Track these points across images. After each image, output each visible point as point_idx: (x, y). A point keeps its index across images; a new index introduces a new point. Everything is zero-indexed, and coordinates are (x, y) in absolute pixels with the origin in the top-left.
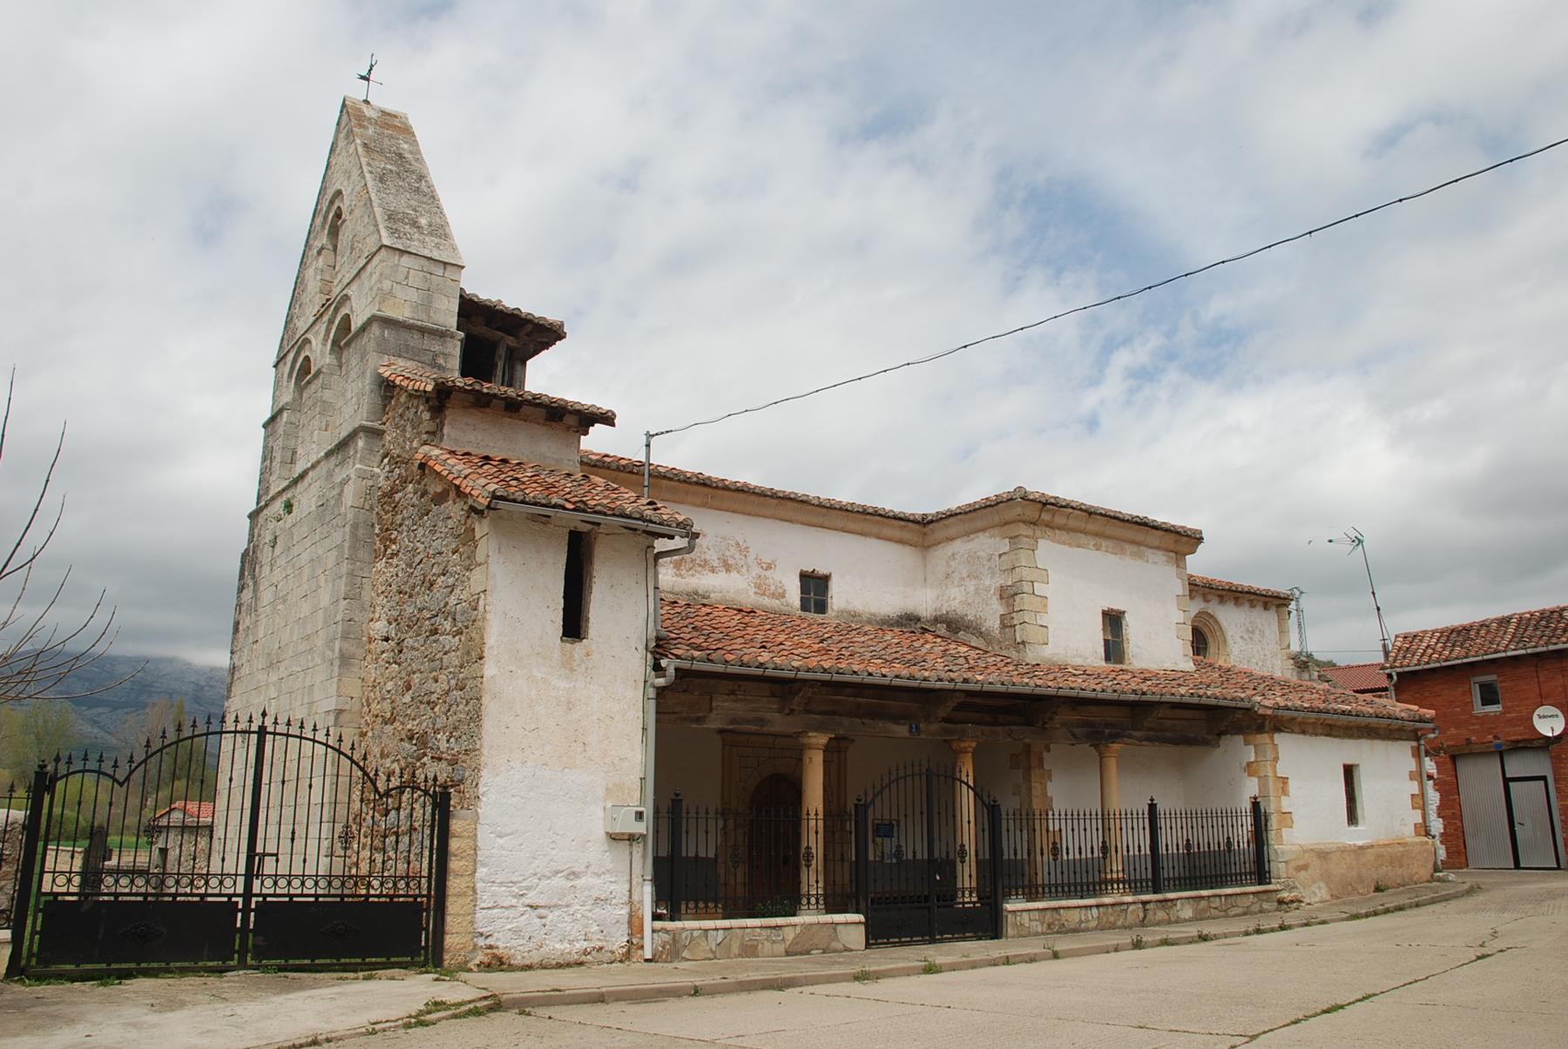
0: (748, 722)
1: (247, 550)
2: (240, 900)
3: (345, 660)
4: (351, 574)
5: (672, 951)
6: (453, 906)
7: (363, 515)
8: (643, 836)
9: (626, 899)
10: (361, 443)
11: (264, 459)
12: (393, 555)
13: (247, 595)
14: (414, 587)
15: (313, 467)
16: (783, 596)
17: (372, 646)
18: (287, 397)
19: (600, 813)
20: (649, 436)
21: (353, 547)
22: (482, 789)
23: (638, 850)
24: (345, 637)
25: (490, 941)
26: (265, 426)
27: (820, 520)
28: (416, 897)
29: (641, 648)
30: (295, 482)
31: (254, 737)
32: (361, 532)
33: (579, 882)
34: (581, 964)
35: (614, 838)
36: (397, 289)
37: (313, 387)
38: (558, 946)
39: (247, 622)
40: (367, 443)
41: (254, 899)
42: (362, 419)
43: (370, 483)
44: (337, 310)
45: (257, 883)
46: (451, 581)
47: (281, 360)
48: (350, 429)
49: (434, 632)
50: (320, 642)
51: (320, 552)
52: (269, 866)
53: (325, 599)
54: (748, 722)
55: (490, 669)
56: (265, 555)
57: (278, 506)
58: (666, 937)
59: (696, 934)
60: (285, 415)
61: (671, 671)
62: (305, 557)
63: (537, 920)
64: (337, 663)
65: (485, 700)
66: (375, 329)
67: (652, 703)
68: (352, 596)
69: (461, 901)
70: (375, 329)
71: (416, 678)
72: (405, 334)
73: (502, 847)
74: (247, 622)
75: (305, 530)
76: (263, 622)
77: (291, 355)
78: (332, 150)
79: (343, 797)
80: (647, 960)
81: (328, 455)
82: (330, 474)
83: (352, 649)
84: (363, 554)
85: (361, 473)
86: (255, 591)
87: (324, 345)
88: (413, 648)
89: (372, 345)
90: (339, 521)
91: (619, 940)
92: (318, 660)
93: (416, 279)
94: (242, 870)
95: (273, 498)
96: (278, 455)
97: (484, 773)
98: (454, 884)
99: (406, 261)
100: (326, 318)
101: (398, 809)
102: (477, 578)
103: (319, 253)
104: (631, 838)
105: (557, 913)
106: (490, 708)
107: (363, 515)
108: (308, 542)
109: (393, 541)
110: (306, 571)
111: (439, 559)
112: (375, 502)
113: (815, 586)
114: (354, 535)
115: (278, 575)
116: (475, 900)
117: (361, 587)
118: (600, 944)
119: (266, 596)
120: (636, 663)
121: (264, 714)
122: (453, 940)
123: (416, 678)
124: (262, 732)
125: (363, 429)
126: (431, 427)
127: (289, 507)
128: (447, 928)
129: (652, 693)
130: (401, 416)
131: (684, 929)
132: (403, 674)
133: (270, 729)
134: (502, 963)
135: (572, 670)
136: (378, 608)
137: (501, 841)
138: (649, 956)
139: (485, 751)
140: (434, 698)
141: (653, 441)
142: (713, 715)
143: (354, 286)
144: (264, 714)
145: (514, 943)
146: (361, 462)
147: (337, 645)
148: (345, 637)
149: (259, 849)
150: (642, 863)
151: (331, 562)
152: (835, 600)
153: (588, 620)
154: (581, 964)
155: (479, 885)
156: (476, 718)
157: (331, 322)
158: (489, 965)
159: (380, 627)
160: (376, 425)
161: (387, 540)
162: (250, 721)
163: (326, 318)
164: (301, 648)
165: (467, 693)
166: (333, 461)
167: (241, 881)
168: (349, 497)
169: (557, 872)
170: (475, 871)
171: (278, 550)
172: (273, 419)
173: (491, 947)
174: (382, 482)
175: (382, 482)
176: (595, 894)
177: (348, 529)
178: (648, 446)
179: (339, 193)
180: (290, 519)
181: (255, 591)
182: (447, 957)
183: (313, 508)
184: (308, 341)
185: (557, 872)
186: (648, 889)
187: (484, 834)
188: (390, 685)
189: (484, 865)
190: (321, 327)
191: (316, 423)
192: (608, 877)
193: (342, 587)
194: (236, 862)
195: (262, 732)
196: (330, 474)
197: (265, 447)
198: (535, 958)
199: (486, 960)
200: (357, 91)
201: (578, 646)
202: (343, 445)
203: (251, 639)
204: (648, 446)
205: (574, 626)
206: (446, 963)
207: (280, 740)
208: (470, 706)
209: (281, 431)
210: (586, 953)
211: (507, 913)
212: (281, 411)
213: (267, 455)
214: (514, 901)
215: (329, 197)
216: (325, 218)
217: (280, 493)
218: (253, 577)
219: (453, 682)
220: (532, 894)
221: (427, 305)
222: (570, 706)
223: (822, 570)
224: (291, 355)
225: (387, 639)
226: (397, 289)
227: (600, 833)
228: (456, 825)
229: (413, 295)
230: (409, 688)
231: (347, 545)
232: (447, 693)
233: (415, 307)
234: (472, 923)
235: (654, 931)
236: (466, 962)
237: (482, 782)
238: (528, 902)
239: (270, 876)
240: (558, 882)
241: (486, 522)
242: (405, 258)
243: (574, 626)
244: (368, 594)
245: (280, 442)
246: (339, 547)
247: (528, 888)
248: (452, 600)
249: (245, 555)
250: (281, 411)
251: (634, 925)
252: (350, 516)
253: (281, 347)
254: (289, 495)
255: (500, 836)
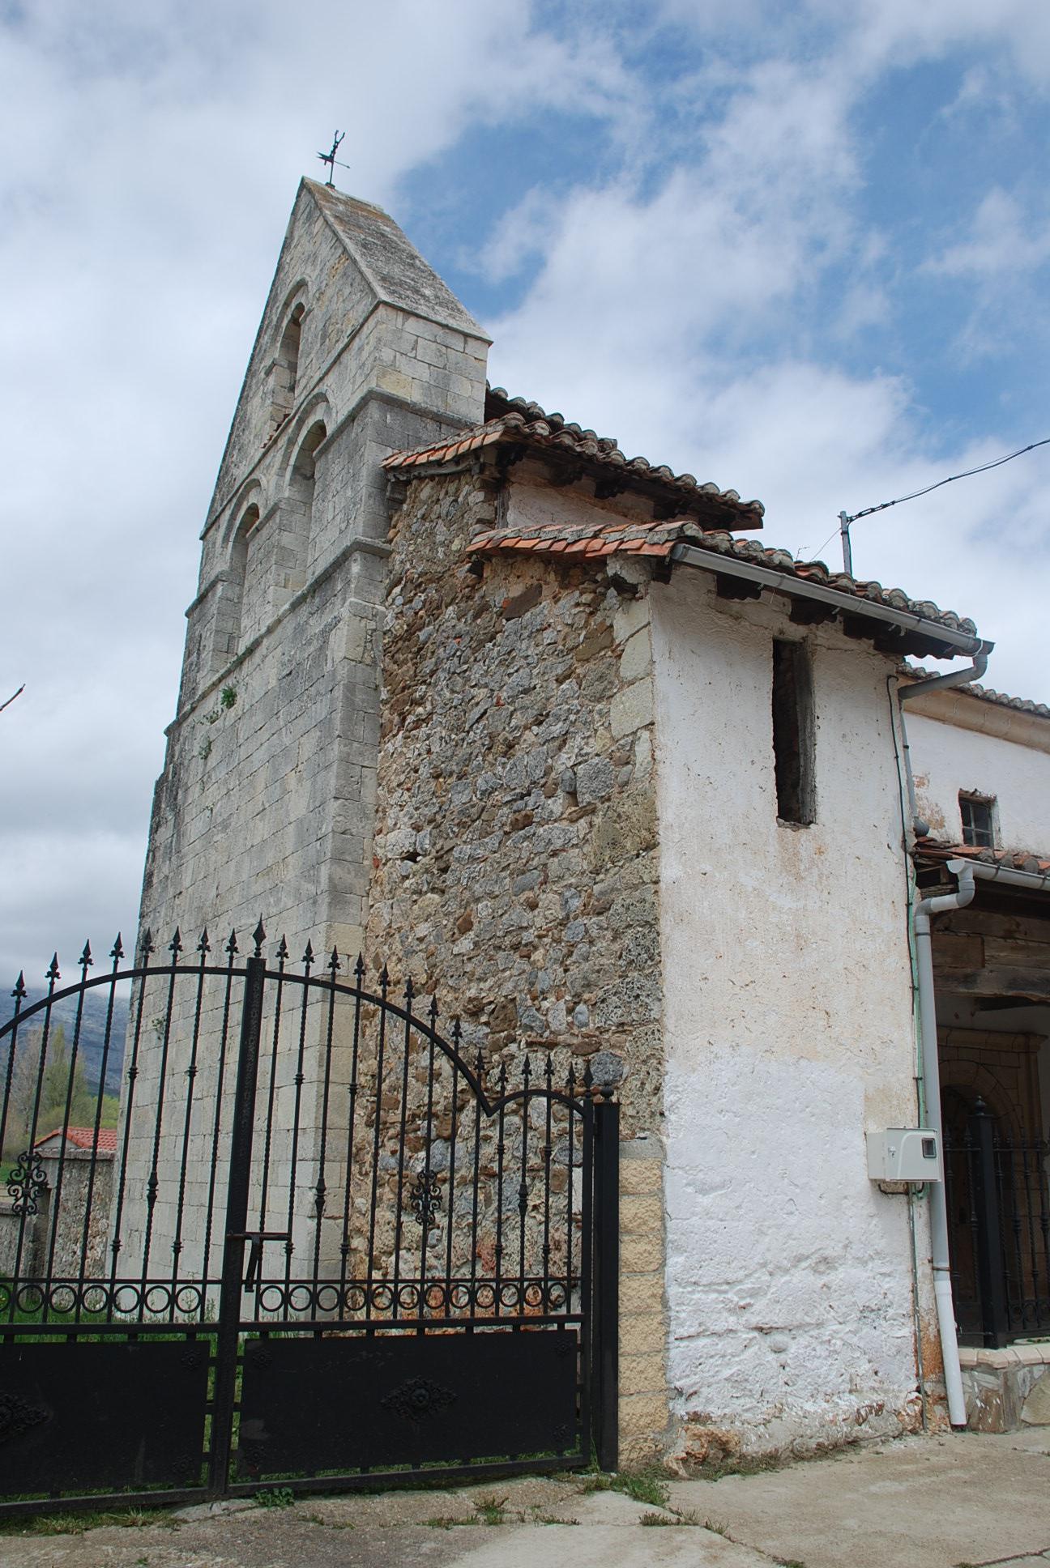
0: (1033, 985)
1: (164, 777)
2: (213, 1337)
3: (338, 895)
4: (346, 760)
5: (997, 1412)
6: (632, 1336)
7: (361, 673)
8: (928, 1187)
9: (908, 1306)
10: (355, 568)
11: (188, 654)
12: (417, 724)
13: (165, 833)
14: (469, 759)
15: (270, 631)
16: (942, 826)
17: (383, 872)
18: (221, 565)
19: (859, 1143)
20: (846, 520)
21: (348, 719)
22: (668, 1098)
23: (920, 1209)
24: (337, 859)
25: (696, 1405)
26: (188, 615)
27: (978, 720)
28: (561, 1320)
29: (896, 844)
30: (240, 662)
31: (239, 983)
32: (359, 697)
33: (836, 1277)
34: (854, 1443)
35: (883, 1189)
36: (401, 362)
37: (265, 532)
38: (809, 1406)
39: (165, 870)
40: (365, 567)
41: (243, 1336)
42: (358, 531)
43: (372, 625)
44: (301, 422)
45: (247, 1300)
46: (557, 729)
47: (211, 524)
48: (338, 551)
49: (524, 822)
50: (290, 873)
51: (287, 741)
52: (273, 1263)
53: (298, 805)
54: (1033, 985)
55: (670, 867)
56: (194, 771)
57: (215, 701)
58: (990, 1382)
59: (1038, 1371)
60: (219, 588)
61: (968, 883)
62: (261, 755)
63: (771, 1356)
64: (324, 900)
65: (665, 925)
66: (374, 411)
67: (925, 942)
68: (347, 795)
69: (642, 1325)
70: (374, 411)
71: (483, 909)
72: (414, 422)
73: (708, 1214)
74: (165, 870)
75: (258, 719)
76: (190, 864)
77: (228, 512)
78: (286, 246)
79: (339, 1119)
80: (955, 1428)
81: (295, 606)
82: (300, 630)
83: (349, 878)
84: (364, 731)
85: (347, 627)
86: (177, 825)
87: (281, 475)
88: (473, 859)
89: (370, 431)
90: (321, 686)
91: (902, 1389)
92: (287, 901)
93: (427, 351)
94: (216, 1270)
95: (204, 696)
96: (209, 643)
97: (669, 1066)
98: (631, 1291)
99: (412, 325)
100: (283, 441)
101: (451, 1139)
102: (624, 712)
103: (268, 373)
104: (909, 1190)
105: (803, 1340)
106: (675, 941)
107: (361, 673)
108: (264, 735)
109: (420, 702)
110: (263, 776)
111: (527, 700)
112: (379, 654)
113: (976, 810)
114: (349, 701)
115: (214, 793)
116: (666, 1322)
117: (360, 782)
118: (877, 1398)
119: (195, 826)
120: (892, 873)
121: (259, 936)
122: (634, 1410)
123: (483, 909)
124: (256, 972)
125: (358, 546)
126: (486, 512)
127: (230, 698)
128: (623, 1384)
129: (923, 923)
130: (424, 518)
131: (1018, 1364)
132: (453, 906)
133: (271, 965)
134: (727, 1454)
135: (799, 878)
136: (391, 813)
137: (705, 1201)
138: (960, 1418)
139: (670, 1023)
140: (529, 936)
141: (852, 527)
142: (985, 972)
143: (330, 379)
144: (259, 936)
145: (737, 1406)
146: (357, 594)
147: (324, 871)
148: (337, 859)
149: (252, 1225)
150: (925, 1233)
151: (309, 745)
152: (1003, 834)
153: (814, 790)
154: (854, 1443)
155: (673, 1291)
156: (644, 957)
157: (291, 442)
158: (704, 1460)
159: (400, 838)
160: (379, 543)
161: (404, 700)
162: (232, 948)
163: (283, 441)
164: (257, 888)
165: (617, 916)
166: (304, 610)
167: (214, 1293)
168: (341, 645)
169: (800, 1259)
170: (663, 1264)
171: (213, 760)
172: (202, 599)
173: (696, 1418)
174: (390, 621)
175: (390, 621)
176: (863, 1298)
177: (339, 692)
178: (845, 533)
179: (301, 285)
180: (232, 713)
181: (177, 825)
182: (623, 1445)
183: (273, 683)
184: (256, 483)
185: (800, 1259)
186: (945, 1286)
187: (675, 1184)
188: (423, 929)
189: (679, 1250)
190: (276, 457)
191: (271, 577)
192: (876, 1265)
193: (331, 780)
194: (203, 1257)
195: (256, 972)
196: (300, 630)
197: (189, 640)
198: (778, 1438)
199: (697, 1448)
200: (319, 174)
201: (803, 834)
202: (324, 581)
203: (171, 892)
204: (845, 533)
205: (794, 802)
206: (623, 1459)
207: (293, 991)
208: (627, 940)
209: (214, 609)
210: (860, 1420)
211: (721, 1345)
212: (213, 585)
213: (193, 646)
214: (732, 1321)
215: (282, 298)
216: (278, 327)
217: (215, 685)
218: (177, 815)
219: (576, 903)
220: (760, 1304)
221: (442, 386)
222: (801, 944)
223: (986, 791)
224: (228, 512)
225: (412, 857)
226: (401, 362)
227: (862, 1184)
228: (630, 1170)
229: (424, 373)
230: (465, 926)
231: (338, 717)
232: (563, 923)
233: (427, 389)
234: (664, 1368)
235: (963, 1368)
236: (659, 1454)
237: (668, 1083)
238: (755, 1320)
239: (273, 1283)
240: (801, 1278)
241: (642, 611)
242: (412, 320)
243: (794, 802)
244: (370, 794)
245: (213, 625)
246: (325, 724)
247: (754, 1293)
248: (565, 759)
249: (159, 784)
250: (213, 585)
251: (930, 1361)
252: (343, 672)
253: (211, 511)
254: (230, 681)
255: (703, 1191)
